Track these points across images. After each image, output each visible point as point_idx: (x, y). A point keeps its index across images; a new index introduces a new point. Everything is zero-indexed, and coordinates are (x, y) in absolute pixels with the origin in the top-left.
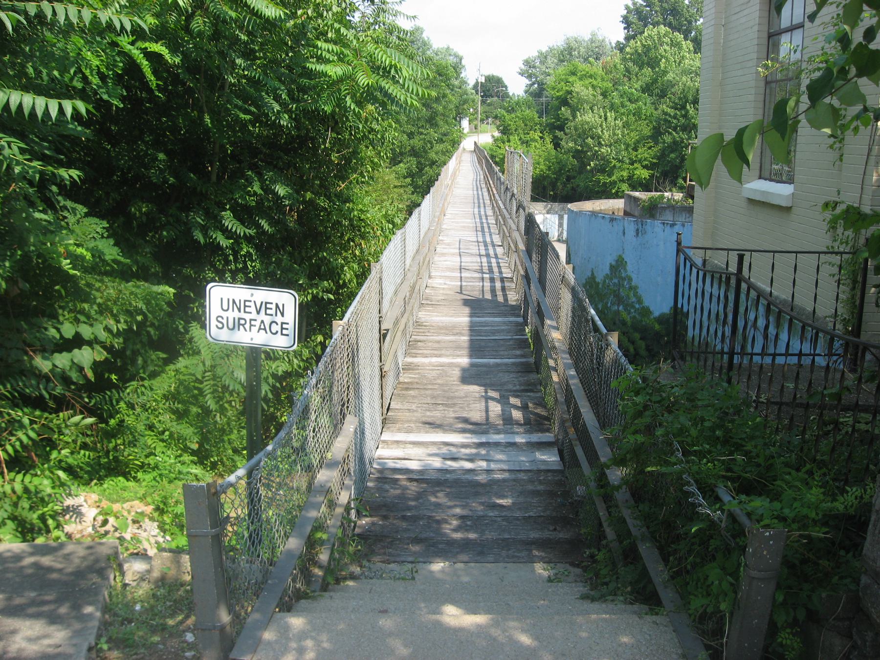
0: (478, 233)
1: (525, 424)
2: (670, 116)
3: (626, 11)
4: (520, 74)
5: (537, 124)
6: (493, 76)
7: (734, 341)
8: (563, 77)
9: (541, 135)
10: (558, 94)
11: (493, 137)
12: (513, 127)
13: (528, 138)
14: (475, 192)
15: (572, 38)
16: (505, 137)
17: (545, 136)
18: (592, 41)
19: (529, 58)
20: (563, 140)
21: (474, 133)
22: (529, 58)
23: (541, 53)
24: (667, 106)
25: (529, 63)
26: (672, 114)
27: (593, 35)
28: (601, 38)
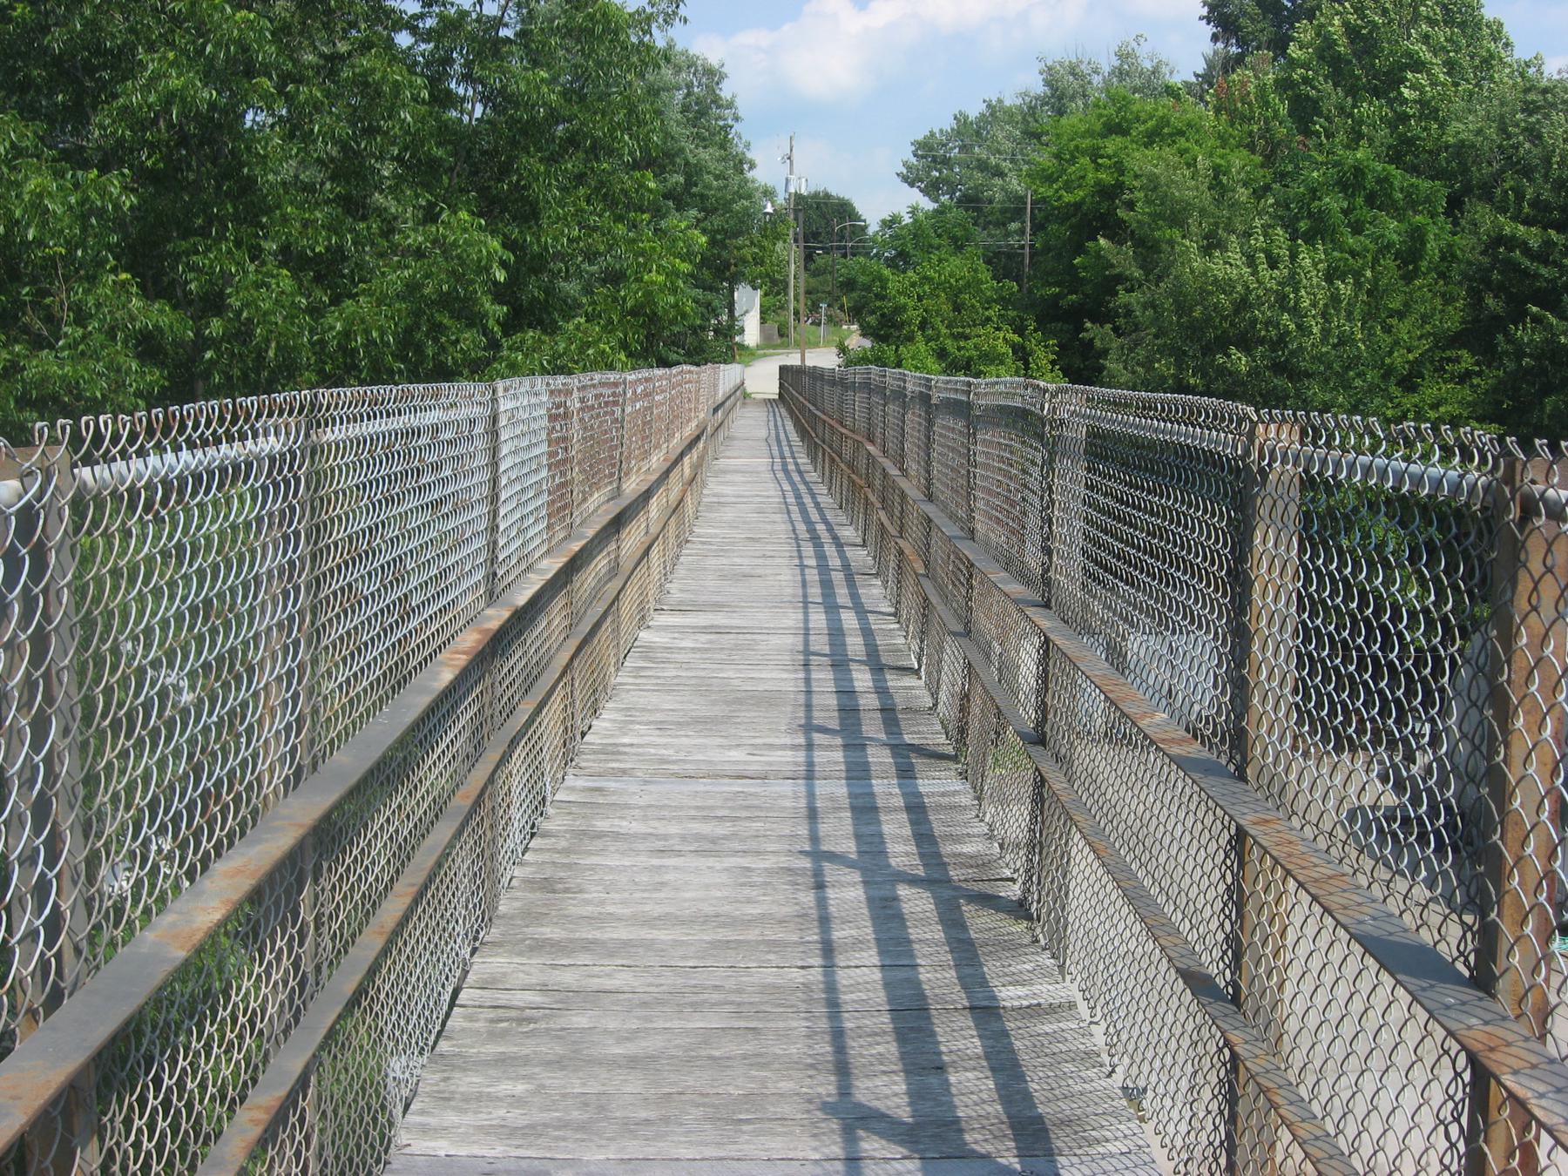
0: (831, 871)
1: (658, 91)
2: (1527, 251)
3: (1206, 8)
4: (905, 179)
5: (990, 301)
6: (827, 196)
7: (793, 490)
8: (1086, 143)
9: (1016, 338)
10: (1068, 198)
11: (843, 350)
12: (913, 315)
13: (969, 349)
14: (818, 619)
15: (1061, 64)
16: (889, 351)
17: (1032, 344)
18: (1121, 74)
19: (932, 134)
20: (1112, 355)
21: (775, 347)
22: (932, 134)
23: (962, 120)
24: (1514, 219)
25: (931, 149)
26: (1534, 243)
27: (1123, 56)
28: (1148, 65)
